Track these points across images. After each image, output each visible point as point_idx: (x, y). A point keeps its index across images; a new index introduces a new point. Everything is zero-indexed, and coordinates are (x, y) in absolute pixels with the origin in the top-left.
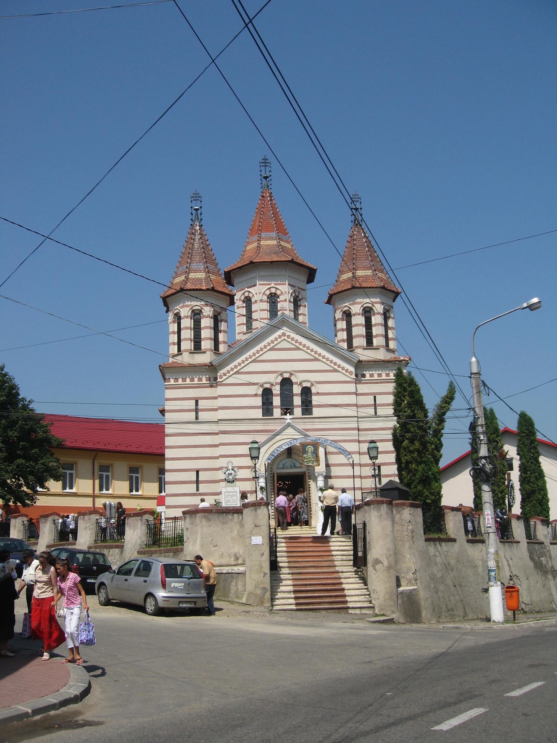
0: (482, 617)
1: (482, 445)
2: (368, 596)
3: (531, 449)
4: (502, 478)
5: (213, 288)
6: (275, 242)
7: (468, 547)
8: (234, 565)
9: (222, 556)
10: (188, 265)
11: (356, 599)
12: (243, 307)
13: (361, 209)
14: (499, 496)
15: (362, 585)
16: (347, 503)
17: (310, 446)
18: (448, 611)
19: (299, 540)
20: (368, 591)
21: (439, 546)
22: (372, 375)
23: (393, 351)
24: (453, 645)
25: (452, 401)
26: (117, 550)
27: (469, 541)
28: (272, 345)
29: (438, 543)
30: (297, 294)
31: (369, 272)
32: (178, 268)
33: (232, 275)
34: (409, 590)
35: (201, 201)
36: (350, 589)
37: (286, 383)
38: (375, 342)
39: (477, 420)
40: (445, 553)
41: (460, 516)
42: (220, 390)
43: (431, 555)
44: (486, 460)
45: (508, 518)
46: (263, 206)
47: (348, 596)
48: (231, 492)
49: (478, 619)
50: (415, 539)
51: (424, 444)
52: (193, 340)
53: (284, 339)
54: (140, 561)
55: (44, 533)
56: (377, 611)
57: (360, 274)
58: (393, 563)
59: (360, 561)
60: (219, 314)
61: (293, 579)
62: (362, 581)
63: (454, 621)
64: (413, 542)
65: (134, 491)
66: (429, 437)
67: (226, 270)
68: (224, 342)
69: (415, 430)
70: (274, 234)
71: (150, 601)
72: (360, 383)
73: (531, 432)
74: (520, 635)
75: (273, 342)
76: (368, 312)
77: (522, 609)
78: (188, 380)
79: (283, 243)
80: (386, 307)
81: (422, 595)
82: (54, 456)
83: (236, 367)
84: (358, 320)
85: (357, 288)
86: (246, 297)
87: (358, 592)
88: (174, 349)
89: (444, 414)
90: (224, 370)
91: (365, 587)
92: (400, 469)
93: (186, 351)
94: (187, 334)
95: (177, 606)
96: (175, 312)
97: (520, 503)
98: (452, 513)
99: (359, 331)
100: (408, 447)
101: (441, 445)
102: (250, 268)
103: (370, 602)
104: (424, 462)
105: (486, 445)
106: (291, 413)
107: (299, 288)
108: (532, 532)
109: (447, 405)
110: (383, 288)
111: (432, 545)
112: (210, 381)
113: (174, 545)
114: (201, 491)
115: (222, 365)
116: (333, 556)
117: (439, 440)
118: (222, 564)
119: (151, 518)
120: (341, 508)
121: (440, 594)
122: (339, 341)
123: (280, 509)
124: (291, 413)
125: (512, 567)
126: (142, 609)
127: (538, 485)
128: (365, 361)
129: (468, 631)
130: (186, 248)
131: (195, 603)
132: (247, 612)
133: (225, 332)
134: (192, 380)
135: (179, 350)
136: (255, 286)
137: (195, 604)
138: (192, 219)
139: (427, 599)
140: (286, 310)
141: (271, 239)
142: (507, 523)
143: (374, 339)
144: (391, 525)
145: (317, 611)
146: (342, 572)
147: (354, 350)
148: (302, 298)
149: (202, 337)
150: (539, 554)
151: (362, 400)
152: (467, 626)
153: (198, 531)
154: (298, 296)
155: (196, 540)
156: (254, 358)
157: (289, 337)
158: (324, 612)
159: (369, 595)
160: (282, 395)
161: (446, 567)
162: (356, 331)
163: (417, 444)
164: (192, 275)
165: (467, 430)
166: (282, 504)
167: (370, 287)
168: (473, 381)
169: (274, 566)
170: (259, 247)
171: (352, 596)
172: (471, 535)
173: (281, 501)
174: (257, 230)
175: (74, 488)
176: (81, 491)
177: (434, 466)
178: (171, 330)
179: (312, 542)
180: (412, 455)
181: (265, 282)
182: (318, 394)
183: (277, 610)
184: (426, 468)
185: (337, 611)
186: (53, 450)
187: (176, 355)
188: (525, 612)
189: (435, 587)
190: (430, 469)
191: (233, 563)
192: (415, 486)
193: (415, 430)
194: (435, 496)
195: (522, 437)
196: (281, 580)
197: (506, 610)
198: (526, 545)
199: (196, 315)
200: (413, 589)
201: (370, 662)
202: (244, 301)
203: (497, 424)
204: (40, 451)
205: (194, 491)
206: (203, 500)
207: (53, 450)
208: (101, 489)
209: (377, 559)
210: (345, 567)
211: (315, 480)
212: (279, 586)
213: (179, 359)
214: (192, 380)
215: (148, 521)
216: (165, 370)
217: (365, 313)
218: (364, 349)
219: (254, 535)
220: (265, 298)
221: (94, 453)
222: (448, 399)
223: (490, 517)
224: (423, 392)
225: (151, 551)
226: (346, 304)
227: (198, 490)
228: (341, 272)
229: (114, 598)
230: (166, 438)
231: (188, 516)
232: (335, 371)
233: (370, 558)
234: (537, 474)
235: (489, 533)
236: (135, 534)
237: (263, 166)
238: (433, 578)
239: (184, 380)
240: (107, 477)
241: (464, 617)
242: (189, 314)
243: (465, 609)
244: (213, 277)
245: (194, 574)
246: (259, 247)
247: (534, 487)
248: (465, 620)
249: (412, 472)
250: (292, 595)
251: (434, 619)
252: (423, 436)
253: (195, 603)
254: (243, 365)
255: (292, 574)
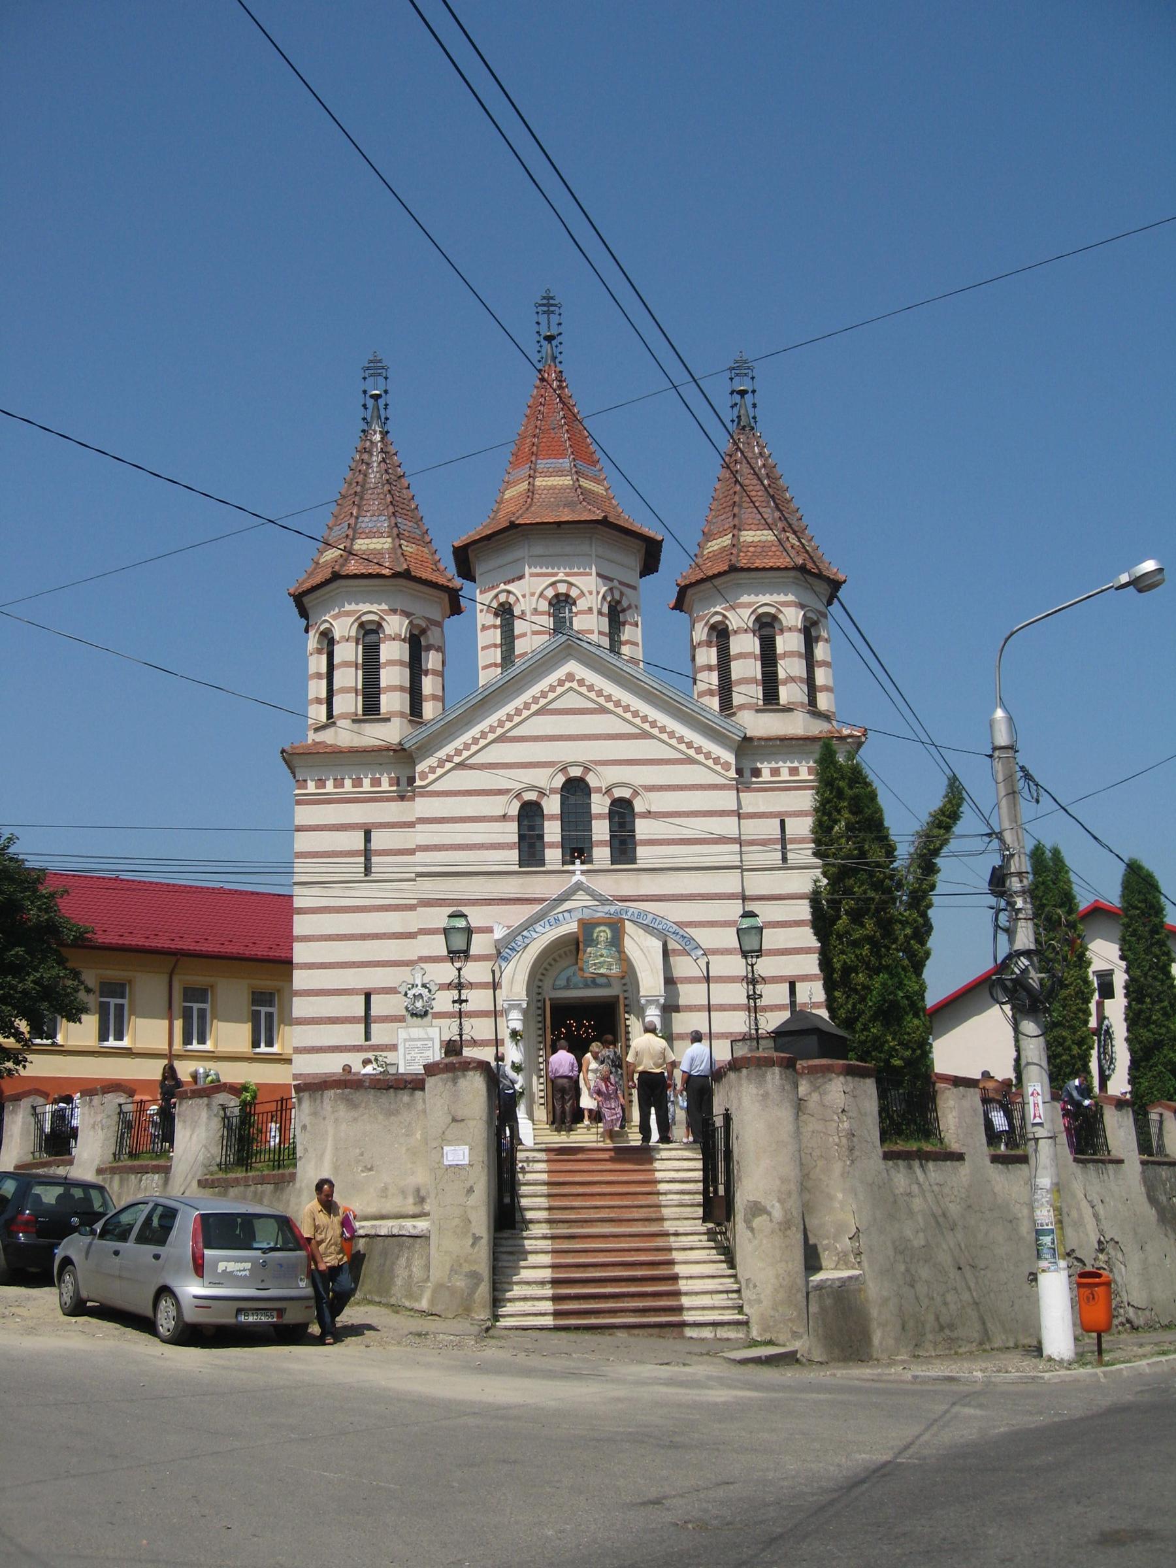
0: (1026, 1341)
1: (1021, 923)
2: (735, 1296)
3: (1152, 945)
4: (1080, 1010)
5: (408, 571)
6: (567, 481)
7: (995, 1173)
8: (414, 1216)
9: (384, 1192)
10: (352, 521)
11: (706, 1301)
12: (495, 627)
13: (754, 392)
14: (1075, 1052)
15: (724, 1266)
16: (701, 1068)
17: (602, 928)
18: (942, 1329)
19: (580, 1156)
20: (737, 1282)
21: (919, 1171)
22: (775, 772)
23: (826, 717)
24: (918, 1437)
25: (955, 823)
26: (156, 1176)
27: (995, 1159)
28: (543, 702)
29: (916, 1164)
30: (617, 597)
31: (767, 536)
32: (330, 529)
33: (471, 555)
34: (839, 1279)
35: (386, 378)
36: (691, 1277)
37: (575, 790)
38: (785, 694)
39: (1009, 860)
40: (935, 1188)
41: (975, 1096)
42: (422, 807)
43: (897, 1192)
44: (1030, 960)
45: (1096, 1104)
46: (542, 400)
47: (686, 1294)
48: (419, 1040)
49: (1016, 1347)
50: (857, 1153)
51: (886, 925)
52: (360, 693)
53: (571, 689)
54: (151, 1205)
55: (12, 1136)
56: (755, 1333)
57: (749, 539)
58: (795, 1213)
59: (717, 1207)
60: (423, 631)
61: (554, 1252)
62: (722, 1258)
63: (956, 1353)
64: (852, 1162)
65: (263, 1045)
66: (900, 909)
67: (456, 544)
68: (434, 697)
69: (865, 892)
70: (566, 463)
71: (165, 1305)
72: (748, 789)
73: (1152, 907)
74: (1105, 1402)
75: (544, 694)
76: (766, 627)
77: (1128, 1321)
78: (348, 783)
79: (584, 483)
80: (809, 615)
81: (875, 1291)
82: (68, 965)
83: (458, 752)
84: (745, 644)
85: (742, 569)
86: (501, 605)
87: (710, 1284)
88: (318, 713)
89: (936, 852)
90: (431, 761)
91: (731, 1272)
92: (829, 987)
93: (344, 716)
94: (348, 678)
95: (232, 1321)
96: (322, 628)
97: (1127, 1071)
98: (955, 1090)
99: (747, 669)
100: (847, 932)
101: (929, 928)
102: (510, 537)
103: (740, 1309)
104: (887, 967)
105: (1030, 924)
106: (588, 860)
107: (621, 583)
108: (1154, 1138)
109: (942, 831)
110: (802, 569)
111: (902, 1169)
112: (398, 785)
113: (279, 1167)
114: (374, 1041)
115: (427, 747)
116: (659, 1193)
117: (924, 915)
118: (384, 1212)
119: (233, 1102)
120: (689, 1079)
121: (921, 1289)
122: (702, 694)
123: (560, 1081)
124: (588, 860)
125: (1103, 1222)
126: (146, 1325)
127: (1168, 1028)
128: (760, 739)
129: (978, 1387)
130: (350, 484)
131: (281, 1312)
132: (419, 1335)
133: (435, 673)
134: (358, 783)
135: (330, 715)
136: (521, 578)
137: (280, 1316)
138: (364, 419)
139: (886, 1300)
140: (592, 632)
141: (559, 473)
142: (1095, 1116)
143: (781, 688)
144: (791, 1119)
145: (607, 1332)
146: (676, 1234)
147: (734, 714)
148: (629, 607)
149: (383, 684)
150: (1171, 1188)
151: (752, 828)
152: (975, 1372)
153: (326, 1131)
154: (618, 602)
155: (322, 1155)
156: (500, 731)
157: (581, 682)
158: (622, 1335)
159: (738, 1291)
160: (564, 817)
161: (937, 1222)
162: (738, 669)
163: (869, 924)
164: (361, 545)
165: (984, 886)
166: (564, 1070)
167: (771, 569)
168: (999, 766)
169: (506, 1218)
170: (531, 491)
171: (697, 1293)
172: (1007, 1145)
173: (560, 1065)
174: (529, 454)
175: (126, 1038)
176: (141, 1045)
177: (910, 979)
178: (312, 669)
179: (611, 1160)
180: (858, 952)
181: (544, 570)
182: (648, 814)
183: (506, 1328)
184: (890, 982)
185: (655, 1331)
186: (65, 952)
187: (324, 727)
188: (1135, 1328)
189: (908, 1270)
190: (900, 985)
191: (411, 1209)
192: (865, 1025)
193: (865, 892)
194: (914, 1051)
195: (1131, 918)
196: (524, 1254)
197: (1080, 1331)
198: (1138, 1167)
199: (370, 634)
200: (850, 1278)
201: (657, 1502)
202: (496, 615)
203: (1069, 882)
204: (26, 952)
205: (361, 1041)
206: (366, 1062)
207: (65, 952)
208: (187, 1040)
209: (756, 1203)
210: (686, 1222)
211: (640, 1013)
212: (516, 1269)
213: (327, 737)
214: (358, 783)
215: (224, 1108)
216: (296, 762)
217: (760, 629)
218: (758, 711)
219: (450, 1143)
220: (544, 606)
221: (170, 959)
222: (946, 819)
223: (1040, 1099)
224: (884, 800)
225: (226, 1180)
226: (718, 609)
227: (368, 1037)
228: (708, 536)
229: (92, 1296)
230: (296, 917)
231: (306, 1095)
232: (690, 761)
233: (743, 1197)
234: (1166, 1004)
235: (1037, 1140)
236: (196, 1138)
237: (544, 312)
238: (902, 1249)
239: (339, 783)
240: (202, 1013)
241: (981, 1344)
242: (353, 633)
243: (984, 1323)
244: (409, 548)
245: (285, 1241)
246: (531, 491)
247: (1161, 1035)
248: (984, 1350)
249: (856, 991)
250: (548, 1291)
251: (903, 1350)
252: (883, 906)
253: (281, 1312)
254: (474, 748)
255: (553, 1238)
